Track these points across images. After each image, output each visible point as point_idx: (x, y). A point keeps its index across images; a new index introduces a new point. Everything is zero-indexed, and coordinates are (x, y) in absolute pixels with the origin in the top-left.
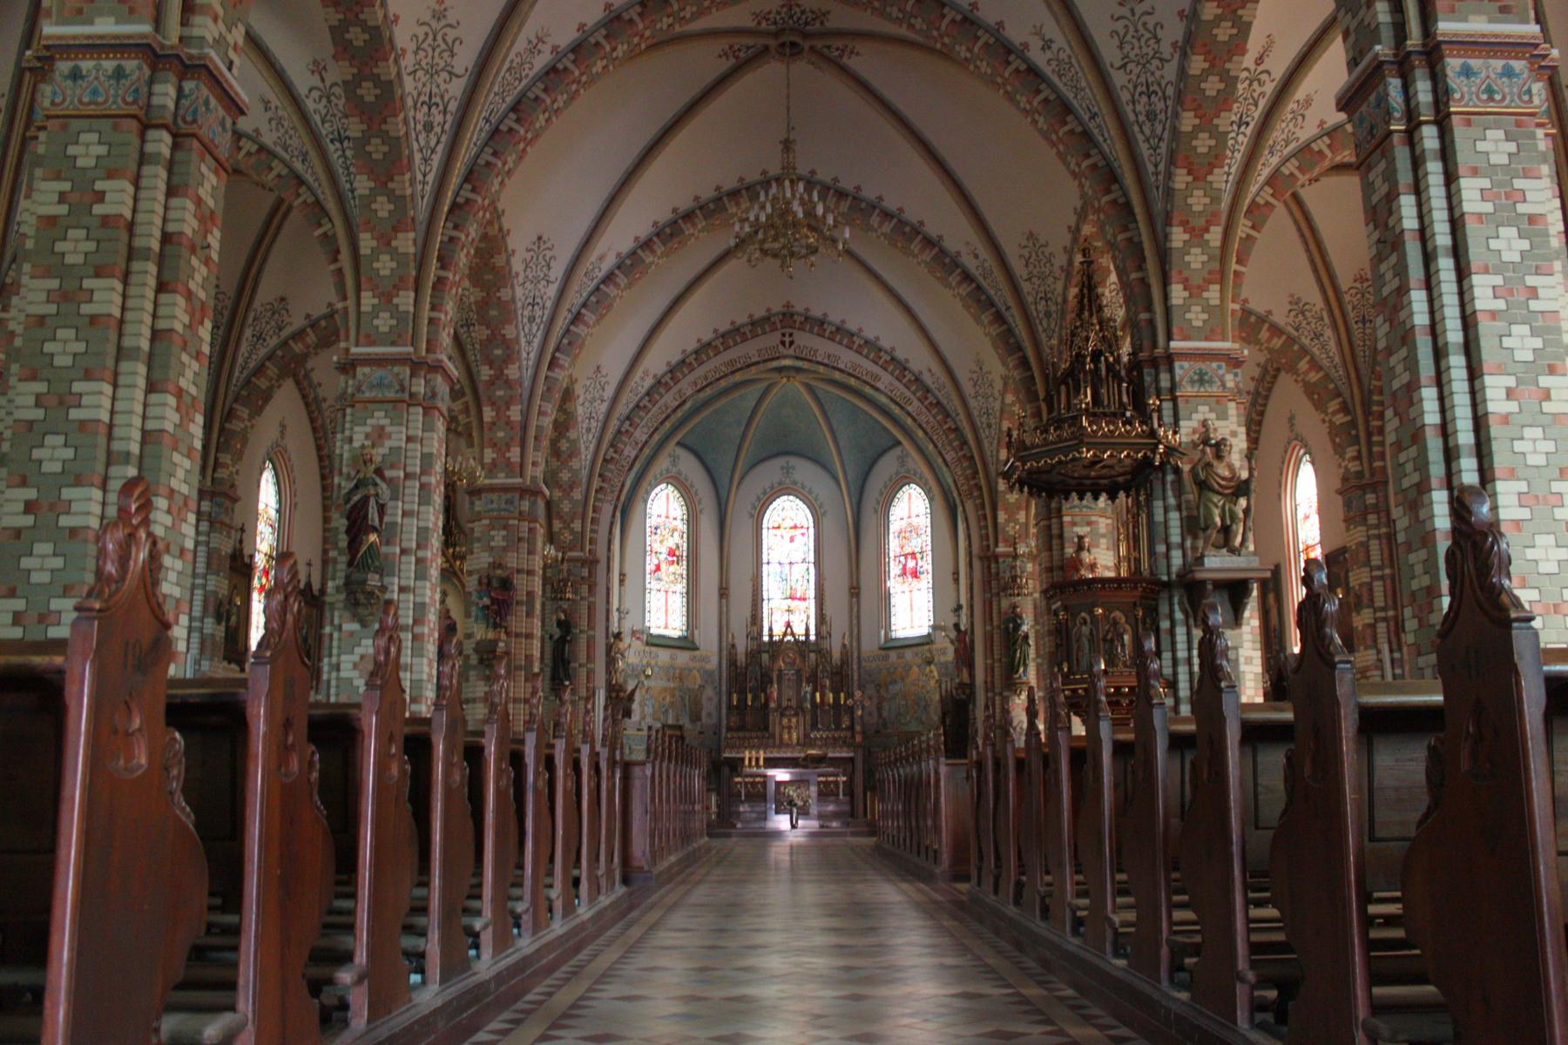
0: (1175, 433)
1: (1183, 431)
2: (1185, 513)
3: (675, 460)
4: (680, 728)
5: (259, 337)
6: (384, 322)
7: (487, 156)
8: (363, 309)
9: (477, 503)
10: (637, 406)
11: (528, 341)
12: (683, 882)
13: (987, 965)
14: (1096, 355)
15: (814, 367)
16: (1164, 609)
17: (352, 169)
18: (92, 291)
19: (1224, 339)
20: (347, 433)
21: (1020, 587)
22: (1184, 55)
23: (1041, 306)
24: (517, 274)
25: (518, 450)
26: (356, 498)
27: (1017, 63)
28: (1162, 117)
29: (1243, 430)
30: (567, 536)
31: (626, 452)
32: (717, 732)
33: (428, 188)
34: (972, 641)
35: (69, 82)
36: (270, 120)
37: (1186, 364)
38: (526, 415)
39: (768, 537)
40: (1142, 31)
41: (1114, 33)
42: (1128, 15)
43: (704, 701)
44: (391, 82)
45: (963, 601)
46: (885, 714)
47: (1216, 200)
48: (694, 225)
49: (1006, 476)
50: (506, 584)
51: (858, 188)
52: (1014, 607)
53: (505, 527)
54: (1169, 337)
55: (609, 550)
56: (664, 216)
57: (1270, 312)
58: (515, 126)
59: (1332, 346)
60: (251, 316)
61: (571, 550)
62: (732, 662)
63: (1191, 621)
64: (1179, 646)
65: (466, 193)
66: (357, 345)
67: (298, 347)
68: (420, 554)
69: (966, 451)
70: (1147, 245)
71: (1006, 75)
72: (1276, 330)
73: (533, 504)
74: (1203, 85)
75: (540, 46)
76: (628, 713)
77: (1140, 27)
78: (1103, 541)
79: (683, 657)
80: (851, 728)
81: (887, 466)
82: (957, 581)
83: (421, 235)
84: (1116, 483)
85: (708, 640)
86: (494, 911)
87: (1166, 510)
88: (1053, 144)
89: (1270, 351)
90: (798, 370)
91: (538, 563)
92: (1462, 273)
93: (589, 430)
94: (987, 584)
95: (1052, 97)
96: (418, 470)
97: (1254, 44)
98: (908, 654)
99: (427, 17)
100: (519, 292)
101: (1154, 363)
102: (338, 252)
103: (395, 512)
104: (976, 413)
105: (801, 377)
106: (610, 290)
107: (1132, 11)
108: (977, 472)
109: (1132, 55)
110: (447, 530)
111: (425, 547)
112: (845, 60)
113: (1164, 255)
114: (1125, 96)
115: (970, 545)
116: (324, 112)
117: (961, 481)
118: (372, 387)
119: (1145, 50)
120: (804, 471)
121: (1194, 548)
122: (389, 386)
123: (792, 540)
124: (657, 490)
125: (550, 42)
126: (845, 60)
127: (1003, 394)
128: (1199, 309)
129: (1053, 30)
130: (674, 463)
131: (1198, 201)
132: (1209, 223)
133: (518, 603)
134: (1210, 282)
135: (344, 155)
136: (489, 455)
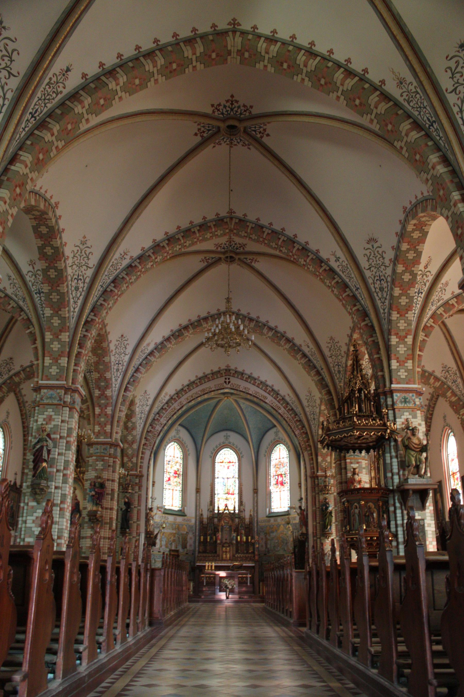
0: (394, 424)
1: (398, 423)
2: (399, 460)
3: (178, 432)
4: (177, 551)
6: (54, 370)
8: (45, 364)
9: (91, 449)
10: (162, 408)
14: (360, 390)
15: (238, 393)
16: (391, 502)
17: (44, 305)
19: (414, 384)
20: (36, 418)
21: (328, 490)
22: (395, 265)
23: (336, 368)
24: (112, 351)
26: (38, 447)
28: (386, 290)
32: (193, 554)
33: (75, 314)
34: (307, 514)
37: (398, 394)
38: (114, 411)
39: (218, 466)
40: (377, 254)
41: (365, 255)
42: (371, 247)
43: (188, 540)
45: (303, 496)
46: (269, 546)
47: (410, 324)
48: (188, 331)
49: (322, 442)
50: (102, 486)
52: (326, 499)
53: (103, 460)
54: (391, 383)
55: (148, 471)
56: (175, 327)
58: (113, 289)
61: (131, 471)
62: (201, 522)
63: (403, 508)
66: (42, 380)
67: (17, 379)
71: (321, 271)
73: (116, 450)
74: (403, 277)
75: (125, 256)
76: (154, 544)
77: (376, 253)
78: (364, 471)
79: (179, 519)
80: (253, 552)
81: (270, 436)
82: (300, 487)
83: (72, 333)
84: (369, 446)
85: (191, 512)
87: (391, 458)
88: (340, 300)
89: (435, 388)
90: (232, 394)
91: (116, 477)
93: (141, 418)
94: (313, 488)
97: (424, 260)
98: (279, 519)
99: (78, 243)
100: (113, 359)
101: (385, 394)
102: (36, 340)
103: (55, 453)
104: (308, 414)
107: (373, 246)
108: (309, 439)
113: (388, 348)
114: (370, 281)
115: (306, 471)
116: (33, 281)
117: (302, 443)
118: (47, 398)
119: (378, 262)
120: (234, 438)
121: (404, 475)
122: (55, 398)
125: (130, 254)
126: (253, 264)
128: (403, 370)
129: (340, 253)
130: (177, 433)
131: (402, 325)
132: (407, 334)
134: (408, 359)
135: (40, 300)
136: (97, 428)
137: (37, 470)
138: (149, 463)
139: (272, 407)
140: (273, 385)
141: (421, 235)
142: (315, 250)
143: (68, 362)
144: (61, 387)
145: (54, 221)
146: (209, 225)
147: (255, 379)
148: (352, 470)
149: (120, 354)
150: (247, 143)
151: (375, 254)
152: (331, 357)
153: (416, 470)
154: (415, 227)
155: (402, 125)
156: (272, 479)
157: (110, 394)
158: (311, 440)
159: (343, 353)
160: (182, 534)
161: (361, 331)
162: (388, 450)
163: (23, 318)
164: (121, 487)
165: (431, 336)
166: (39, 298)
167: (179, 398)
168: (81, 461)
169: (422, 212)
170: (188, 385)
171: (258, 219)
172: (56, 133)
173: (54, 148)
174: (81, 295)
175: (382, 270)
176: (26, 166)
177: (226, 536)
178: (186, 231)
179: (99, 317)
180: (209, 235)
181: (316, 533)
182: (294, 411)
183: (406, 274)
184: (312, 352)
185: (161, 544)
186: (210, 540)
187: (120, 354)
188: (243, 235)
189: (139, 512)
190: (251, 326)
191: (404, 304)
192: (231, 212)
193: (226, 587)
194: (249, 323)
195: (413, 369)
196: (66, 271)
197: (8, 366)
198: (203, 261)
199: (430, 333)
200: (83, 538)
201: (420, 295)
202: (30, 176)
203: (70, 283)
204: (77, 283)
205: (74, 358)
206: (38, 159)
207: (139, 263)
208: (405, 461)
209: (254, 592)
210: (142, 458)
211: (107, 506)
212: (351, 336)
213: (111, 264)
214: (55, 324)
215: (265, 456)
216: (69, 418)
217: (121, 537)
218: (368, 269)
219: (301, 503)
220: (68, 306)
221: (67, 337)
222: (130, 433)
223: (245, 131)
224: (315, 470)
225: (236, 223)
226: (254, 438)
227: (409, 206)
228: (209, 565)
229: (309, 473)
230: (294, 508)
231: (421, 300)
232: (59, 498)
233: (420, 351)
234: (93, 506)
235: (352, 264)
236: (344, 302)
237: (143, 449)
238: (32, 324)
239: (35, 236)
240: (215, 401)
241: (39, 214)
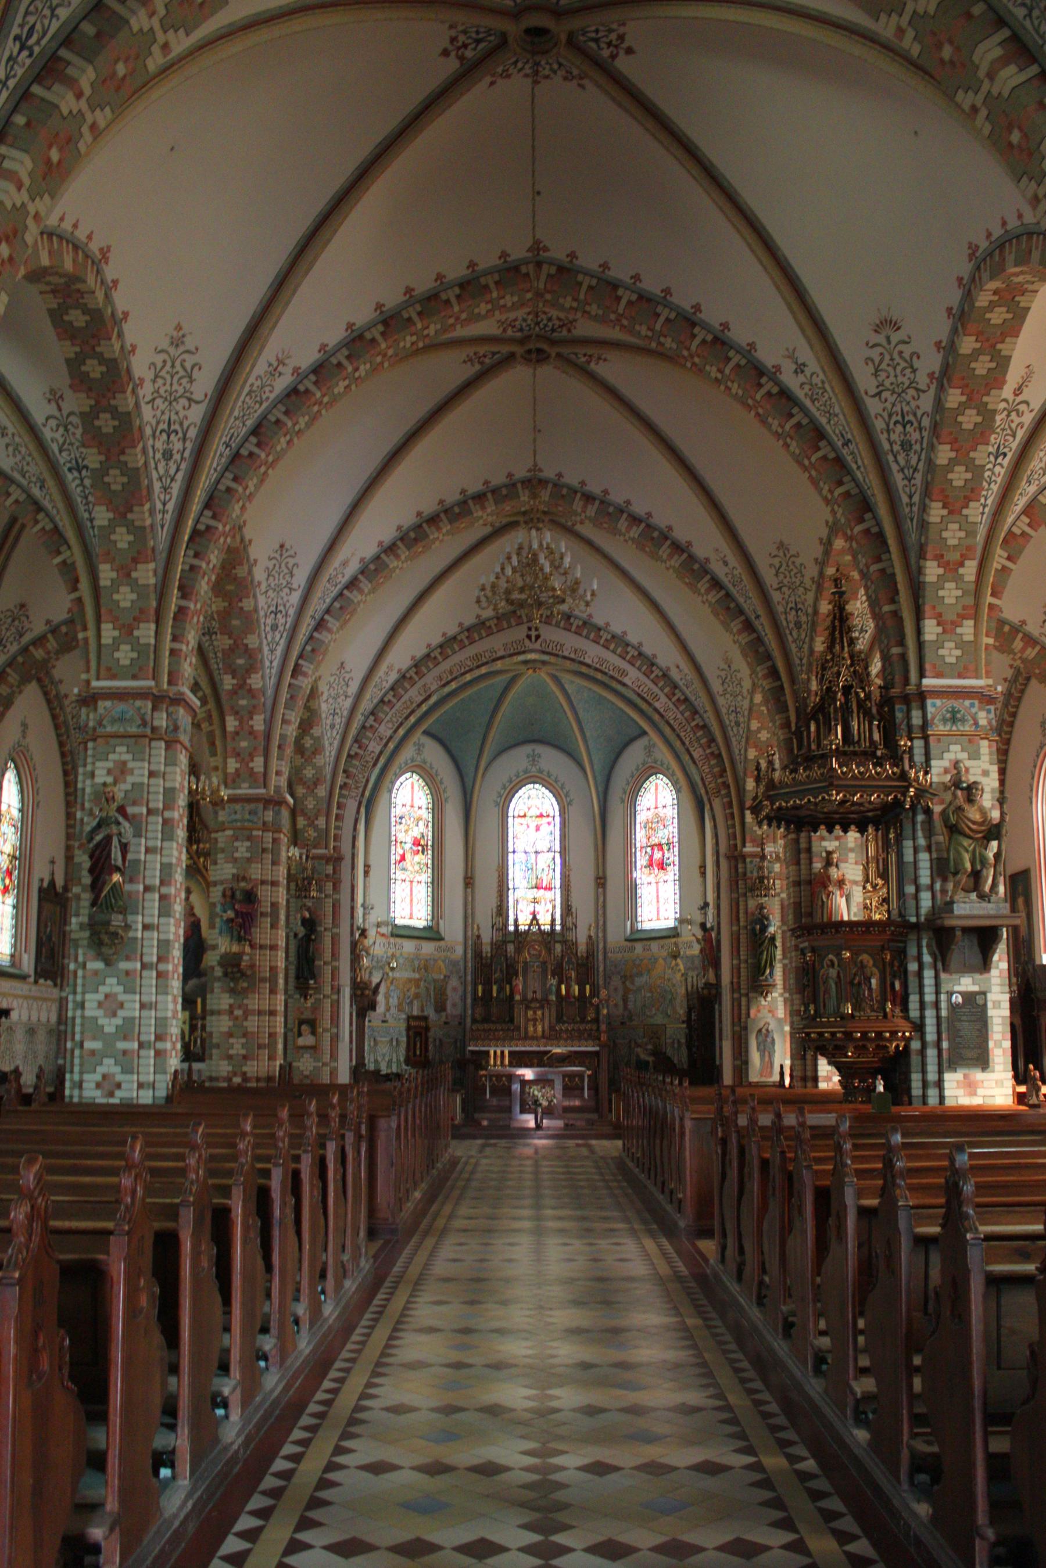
0: (926, 773)
1: (934, 771)
2: (934, 856)
3: (420, 748)
4: (425, 1018)
6: (125, 655)
7: (227, 482)
8: (103, 641)
9: (221, 813)
10: (382, 701)
11: (270, 649)
12: (426, 1234)
13: (728, 1408)
14: (847, 690)
15: (560, 661)
16: (912, 951)
17: (91, 498)
19: (977, 677)
20: (89, 768)
21: (767, 889)
22: (941, 388)
24: (259, 583)
25: (262, 759)
26: (98, 838)
27: (769, 386)
28: (917, 447)
30: (312, 833)
31: (370, 748)
32: (462, 1023)
33: (168, 517)
34: (719, 941)
36: (7, 446)
37: (938, 702)
38: (269, 724)
39: (515, 827)
40: (897, 359)
41: (869, 360)
42: (885, 343)
43: (449, 992)
44: (129, 413)
45: (710, 898)
46: (631, 1006)
47: (971, 533)
48: (439, 529)
49: (756, 810)
50: (250, 897)
51: (606, 492)
52: (761, 907)
53: (249, 838)
54: (922, 675)
55: (354, 846)
56: (408, 519)
57: (1024, 622)
58: (256, 450)
61: (315, 847)
62: (478, 954)
63: (940, 965)
64: (927, 990)
65: (207, 520)
66: (98, 679)
67: (39, 654)
68: (164, 890)
70: (900, 578)
71: (758, 397)
72: (1030, 640)
73: (277, 813)
74: (960, 419)
75: (280, 368)
76: (373, 1006)
77: (896, 356)
78: (852, 856)
79: (428, 948)
80: (596, 1020)
81: (634, 756)
82: (703, 874)
83: (162, 565)
84: (867, 817)
85: (453, 930)
86: (242, 1374)
87: (916, 850)
88: (805, 469)
89: (1024, 661)
90: (544, 663)
91: (282, 872)
93: (332, 726)
94: (734, 883)
95: (805, 422)
96: (161, 806)
97: (1013, 376)
98: (654, 946)
99: (165, 344)
100: (262, 601)
101: (906, 699)
102: (77, 580)
103: (138, 851)
104: (724, 711)
105: (545, 669)
106: (355, 596)
107: (888, 338)
108: (725, 771)
109: (887, 383)
110: (191, 829)
111: (169, 884)
112: (592, 366)
113: (917, 589)
114: (879, 425)
115: (717, 843)
116: (61, 441)
117: (709, 779)
118: (114, 721)
119: (900, 379)
120: (550, 759)
121: (944, 891)
122: (131, 721)
123: (538, 829)
124: (402, 779)
125: (292, 363)
126: (592, 366)
127: (752, 693)
128: (952, 645)
129: (806, 354)
130: (419, 751)
131: (953, 535)
132: (964, 557)
133: (262, 914)
134: (964, 617)
135: (82, 484)
136: (232, 765)
137: (101, 891)
138: (355, 829)
139: (639, 695)
140: (640, 644)
141: (1010, 316)
142: (744, 345)
143: (157, 632)
144: (142, 695)
145: (100, 295)
146: (483, 281)
147: (600, 629)
148: (824, 854)
149: (278, 589)
150: (575, 72)
151: (892, 359)
152: (780, 589)
153: (972, 880)
154: (996, 298)
155: (981, 48)
156: (638, 854)
157: (260, 685)
158: (729, 773)
159: (808, 582)
160: (435, 981)
161: (854, 544)
162: (910, 832)
163: (43, 528)
164: (293, 886)
165: (1023, 560)
166: (78, 482)
168: (198, 827)
170: (441, 646)
171: (605, 266)
172: (87, 91)
173: (85, 130)
174: (178, 470)
175: (908, 398)
176: (19, 186)
177: (534, 984)
178: (429, 299)
179: (224, 519)
180: (483, 308)
181: (739, 983)
182: (691, 704)
183: (968, 412)
184: (733, 576)
185: (387, 1003)
186: (498, 992)
188: (567, 305)
189: (335, 940)
190: (588, 513)
191: (961, 483)
192: (537, 247)
193: (536, 1102)
194: (585, 507)
195: (976, 642)
196: (139, 415)
197: (16, 623)
198: (471, 360)
199: (1021, 552)
200: (212, 1013)
201: (999, 460)
202: (31, 209)
203: (151, 442)
204: (168, 442)
205: (170, 623)
206: (48, 161)
207: (316, 383)
208: (948, 859)
209: (597, 1110)
210: (338, 817)
211: (263, 942)
212: (827, 544)
213: (246, 390)
214: (120, 545)
215: (623, 801)
216: (166, 765)
217: (297, 996)
218: (874, 396)
219: (705, 914)
220: (149, 497)
221: (151, 574)
222: (308, 761)
223: (571, 42)
224: (739, 842)
225: (549, 276)
226: (595, 762)
227: (984, 245)
228: (498, 1053)
229: (723, 849)
230: (689, 922)
231: (1003, 471)
232: (155, 950)
233: (993, 595)
234: (231, 945)
235: (839, 388)
236: (813, 473)
237: (341, 795)
238: (66, 543)
239: (58, 334)
240: (507, 677)
241: (62, 280)
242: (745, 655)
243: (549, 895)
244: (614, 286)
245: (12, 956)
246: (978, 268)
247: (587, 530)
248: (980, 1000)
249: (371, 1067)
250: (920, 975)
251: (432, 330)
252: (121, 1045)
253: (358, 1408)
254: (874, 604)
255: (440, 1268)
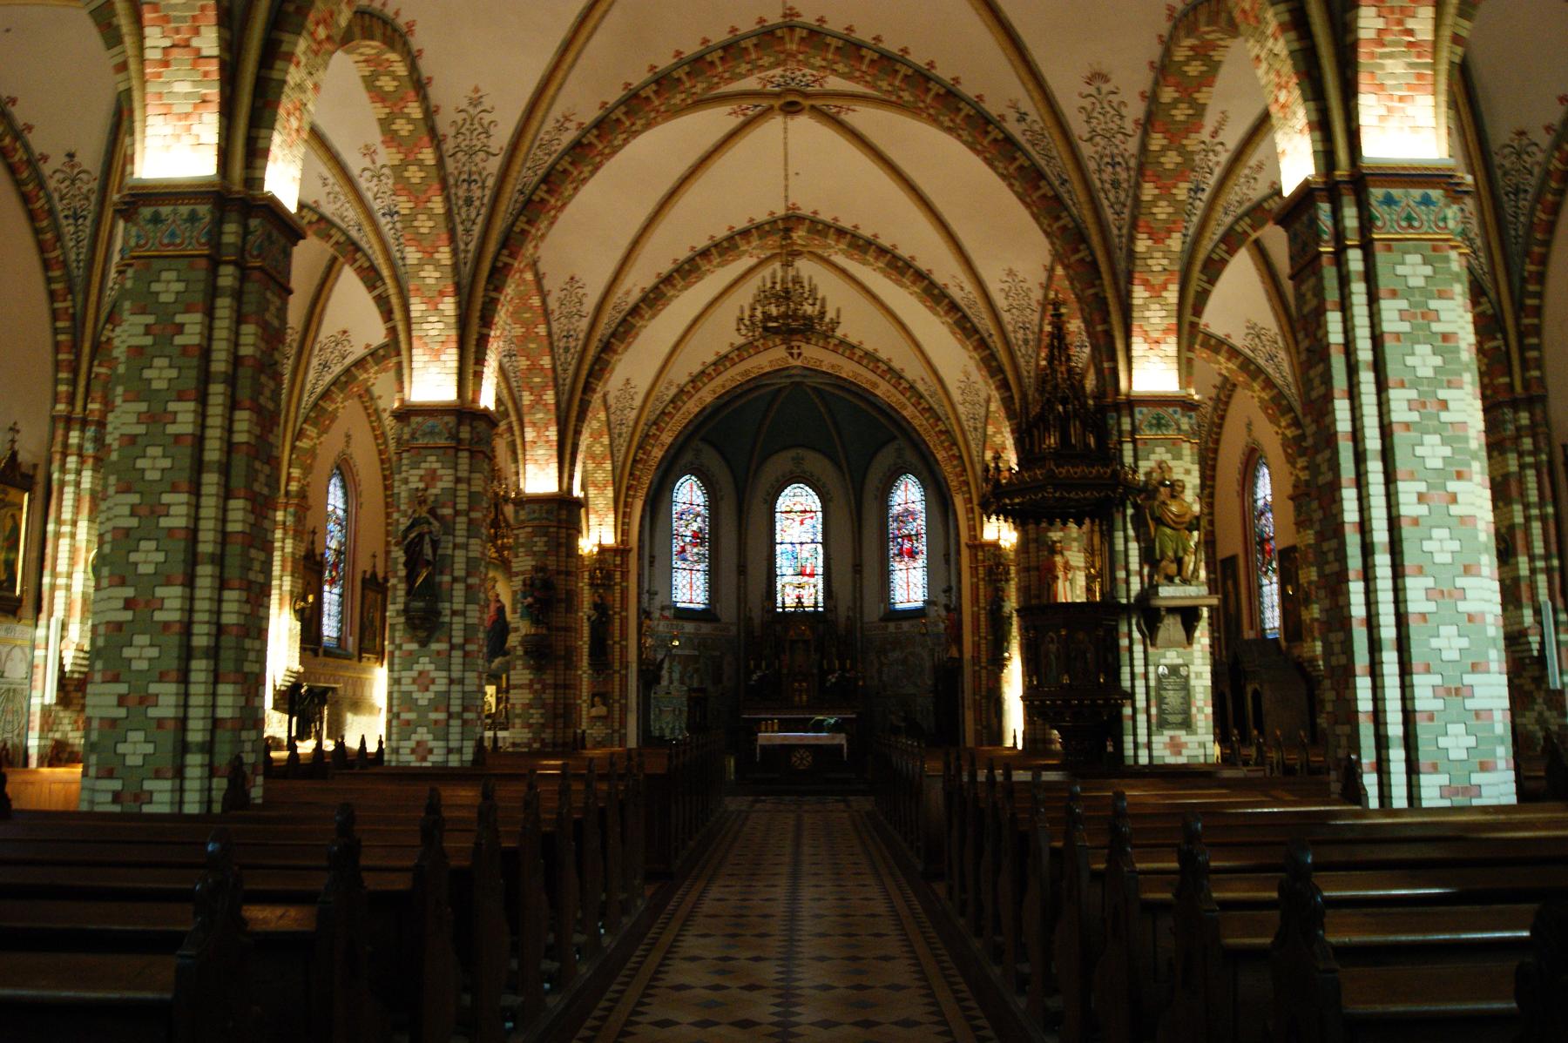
5: (325, 365)
16: (1124, 629)
18: (175, 413)
23: (1020, 335)
29: (1196, 467)
35: (150, 227)
37: (1145, 410)
39: (781, 522)
42: (1094, 93)
46: (885, 678)
59: (1286, 366)
60: (317, 347)
69: (955, 451)
76: (658, 679)
79: (706, 628)
85: (728, 612)
92: (1381, 386)
97: (1210, 122)
98: (906, 625)
99: (464, 104)
104: (963, 418)
107: (1098, 89)
108: (965, 470)
114: (1092, 166)
118: (424, 435)
119: (1111, 125)
121: (1151, 576)
122: (440, 434)
123: (802, 523)
126: (843, 116)
167: (698, 390)
169: (1208, 25)
170: (715, 364)
180: (744, 68)
187: (569, 316)
204: (469, 190)
213: (537, 143)
237: (627, 496)
238: (382, 279)
242: (979, 370)
243: (812, 580)
244: (859, 46)
245: (339, 639)
246: (1175, 27)
247: (840, 260)
248: (1183, 671)
249: (657, 734)
250: (1130, 650)
251: (699, 88)
252: (411, 716)
253: (629, 1023)
254: (1089, 324)
255: (708, 906)
